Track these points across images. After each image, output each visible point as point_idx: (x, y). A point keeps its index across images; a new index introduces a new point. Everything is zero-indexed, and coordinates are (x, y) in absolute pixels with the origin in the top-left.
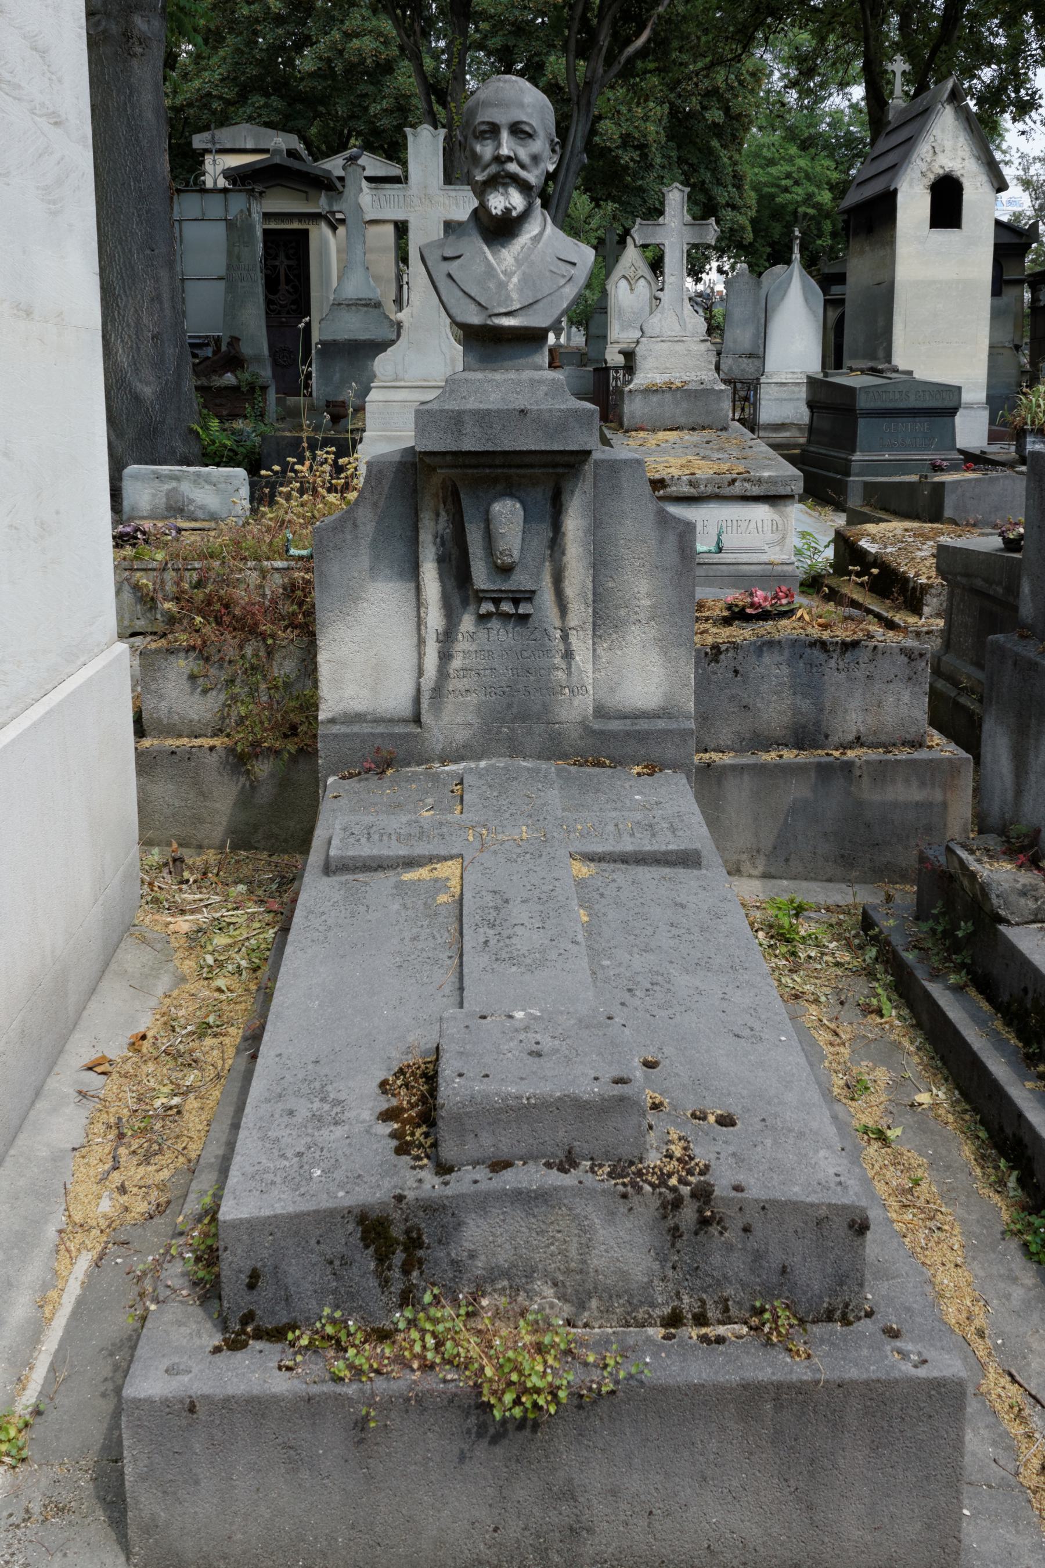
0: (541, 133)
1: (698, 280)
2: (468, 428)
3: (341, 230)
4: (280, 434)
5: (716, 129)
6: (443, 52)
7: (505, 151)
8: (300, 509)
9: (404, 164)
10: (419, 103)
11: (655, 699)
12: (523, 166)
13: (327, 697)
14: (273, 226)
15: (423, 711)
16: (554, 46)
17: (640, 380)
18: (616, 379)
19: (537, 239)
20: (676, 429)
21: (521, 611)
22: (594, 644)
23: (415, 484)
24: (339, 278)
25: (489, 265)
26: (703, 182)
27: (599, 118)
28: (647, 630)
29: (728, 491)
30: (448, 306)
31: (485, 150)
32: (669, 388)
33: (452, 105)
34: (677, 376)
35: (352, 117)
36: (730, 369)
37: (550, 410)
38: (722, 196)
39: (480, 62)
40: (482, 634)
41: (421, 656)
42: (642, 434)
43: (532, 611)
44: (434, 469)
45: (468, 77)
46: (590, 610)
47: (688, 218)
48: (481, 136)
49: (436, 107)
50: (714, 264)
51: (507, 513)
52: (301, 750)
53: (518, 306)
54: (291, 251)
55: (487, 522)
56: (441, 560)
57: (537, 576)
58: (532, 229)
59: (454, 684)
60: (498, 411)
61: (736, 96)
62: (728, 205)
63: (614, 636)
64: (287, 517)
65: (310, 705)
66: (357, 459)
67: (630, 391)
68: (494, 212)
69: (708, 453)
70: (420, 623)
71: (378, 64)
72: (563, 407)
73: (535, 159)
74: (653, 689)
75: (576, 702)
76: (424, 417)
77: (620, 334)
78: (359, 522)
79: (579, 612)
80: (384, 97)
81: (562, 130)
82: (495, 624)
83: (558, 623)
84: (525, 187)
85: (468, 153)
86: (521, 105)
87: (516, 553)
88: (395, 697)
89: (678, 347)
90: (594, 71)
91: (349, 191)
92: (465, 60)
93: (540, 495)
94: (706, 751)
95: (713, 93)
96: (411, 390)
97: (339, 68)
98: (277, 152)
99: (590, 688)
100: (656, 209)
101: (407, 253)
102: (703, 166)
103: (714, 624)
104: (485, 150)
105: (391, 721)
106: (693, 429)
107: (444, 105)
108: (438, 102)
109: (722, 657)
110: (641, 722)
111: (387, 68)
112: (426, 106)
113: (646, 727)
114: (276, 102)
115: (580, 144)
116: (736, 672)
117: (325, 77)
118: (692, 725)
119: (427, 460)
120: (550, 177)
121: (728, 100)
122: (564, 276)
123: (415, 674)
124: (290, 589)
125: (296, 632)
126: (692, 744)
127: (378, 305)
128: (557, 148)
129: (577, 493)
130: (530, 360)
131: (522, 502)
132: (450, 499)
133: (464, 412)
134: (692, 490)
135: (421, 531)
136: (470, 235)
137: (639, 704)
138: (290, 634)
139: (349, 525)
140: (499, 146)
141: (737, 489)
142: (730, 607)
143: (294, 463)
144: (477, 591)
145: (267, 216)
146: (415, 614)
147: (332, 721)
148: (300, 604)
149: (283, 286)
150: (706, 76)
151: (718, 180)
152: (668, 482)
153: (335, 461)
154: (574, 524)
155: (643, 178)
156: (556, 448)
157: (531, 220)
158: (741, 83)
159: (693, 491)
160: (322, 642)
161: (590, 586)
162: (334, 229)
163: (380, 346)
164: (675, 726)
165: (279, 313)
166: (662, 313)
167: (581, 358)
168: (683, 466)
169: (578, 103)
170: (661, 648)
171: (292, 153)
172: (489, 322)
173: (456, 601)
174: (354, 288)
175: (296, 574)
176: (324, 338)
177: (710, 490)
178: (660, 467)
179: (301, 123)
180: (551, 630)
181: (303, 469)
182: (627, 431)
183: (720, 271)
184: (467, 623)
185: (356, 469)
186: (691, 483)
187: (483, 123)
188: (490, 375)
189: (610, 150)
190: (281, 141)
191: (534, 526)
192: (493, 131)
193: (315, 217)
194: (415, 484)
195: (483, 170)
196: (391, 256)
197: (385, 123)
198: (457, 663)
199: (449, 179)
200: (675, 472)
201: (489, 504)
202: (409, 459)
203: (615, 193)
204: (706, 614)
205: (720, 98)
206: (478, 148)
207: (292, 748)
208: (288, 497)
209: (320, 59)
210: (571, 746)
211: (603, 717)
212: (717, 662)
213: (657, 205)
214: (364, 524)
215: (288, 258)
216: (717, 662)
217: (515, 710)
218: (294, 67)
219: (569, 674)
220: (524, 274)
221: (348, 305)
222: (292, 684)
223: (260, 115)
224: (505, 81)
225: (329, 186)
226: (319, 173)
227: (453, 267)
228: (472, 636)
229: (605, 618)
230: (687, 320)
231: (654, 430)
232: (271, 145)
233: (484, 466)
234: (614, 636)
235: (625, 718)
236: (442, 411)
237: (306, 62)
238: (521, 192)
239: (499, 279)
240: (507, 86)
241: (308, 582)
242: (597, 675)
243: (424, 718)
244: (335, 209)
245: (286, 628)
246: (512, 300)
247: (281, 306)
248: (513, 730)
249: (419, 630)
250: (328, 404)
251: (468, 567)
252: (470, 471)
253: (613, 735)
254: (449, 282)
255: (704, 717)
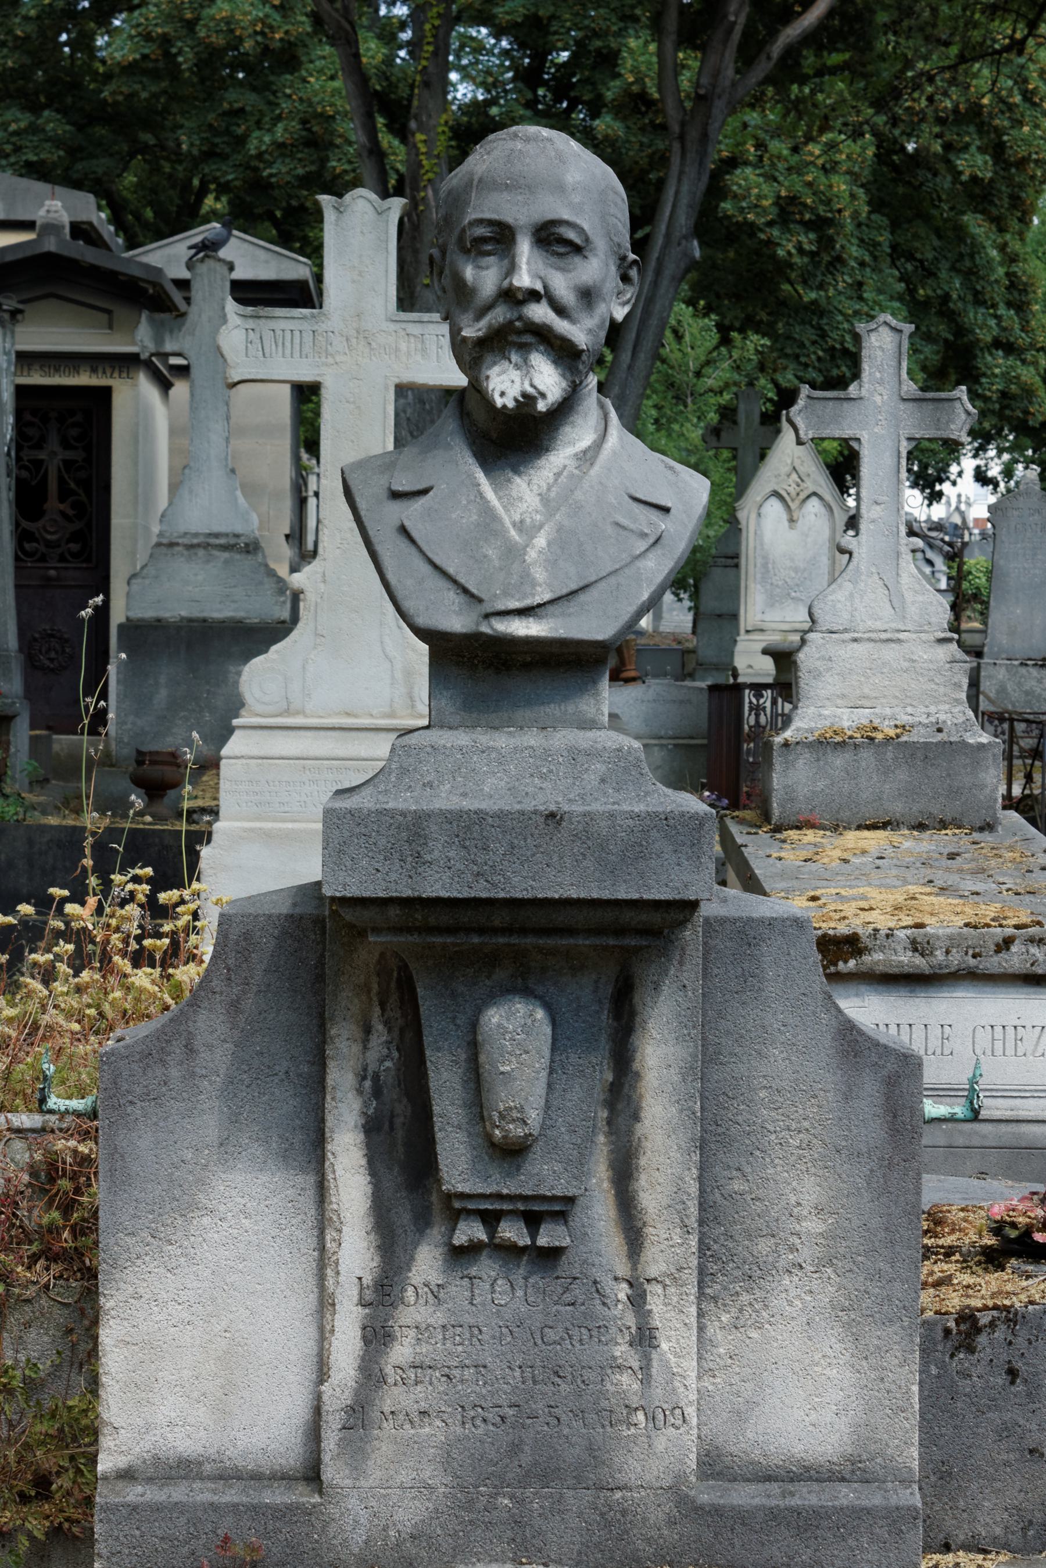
0: (600, 244)
1: (935, 497)
2: (437, 850)
3: (180, 389)
4: (36, 818)
5: (978, 195)
6: (403, 26)
7: (524, 279)
8: (74, 1002)
9: (314, 251)
10: (350, 129)
11: (834, 1438)
12: (561, 311)
13: (117, 1422)
14: (37, 379)
15: (326, 1458)
16: (636, 19)
17: (808, 720)
18: (757, 709)
19: (588, 457)
20: (884, 826)
21: (542, 1241)
22: (701, 1314)
23: (321, 963)
24: (174, 488)
25: (487, 511)
26: (946, 298)
27: (732, 163)
28: (815, 1285)
29: (994, 963)
30: (399, 595)
31: (484, 277)
32: (868, 738)
33: (420, 137)
34: (887, 715)
35: (210, 154)
36: (1002, 690)
37: (612, 815)
38: (983, 326)
39: (479, 48)
40: (458, 1289)
41: (323, 1335)
42: (810, 836)
43: (566, 1242)
44: (362, 933)
45: (454, 76)
46: (694, 1242)
47: (910, 388)
48: (475, 248)
49: (387, 140)
50: (969, 464)
51: (517, 1033)
52: (56, 1532)
53: (547, 597)
54: (74, 432)
55: (474, 1047)
56: (373, 1128)
57: (579, 1166)
58: (578, 436)
59: (394, 1398)
60: (501, 815)
61: (1019, 123)
62: (997, 344)
63: (745, 1298)
64: (45, 1019)
65: (81, 1433)
66: (197, 894)
67: (786, 744)
68: (499, 402)
69: (953, 879)
70: (324, 1262)
71: (266, 51)
72: (639, 808)
73: (588, 295)
74: (828, 1416)
75: (660, 1443)
76: (346, 827)
77: (765, 615)
78: (198, 1043)
79: (668, 1246)
80: (279, 118)
81: (642, 217)
82: (486, 1267)
83: (622, 1269)
84: (565, 353)
85: (446, 281)
86: (560, 188)
87: (534, 1116)
88: (265, 1426)
89: (890, 653)
90: (716, 74)
91: (200, 311)
92: (447, 46)
93: (587, 992)
94: (947, 1548)
95: (972, 115)
96: (313, 756)
97: (186, 59)
98: (51, 228)
99: (691, 1411)
100: (846, 352)
101: (317, 431)
102: (945, 265)
103: (965, 1265)
104: (484, 277)
105: (256, 1477)
106: (921, 827)
107: (403, 134)
108: (390, 128)
109: (982, 1339)
110: (803, 1488)
111: (287, 58)
112: (363, 139)
113: (813, 1500)
114: (52, 122)
115: (684, 221)
116: (1013, 1373)
117: (155, 75)
118: (912, 1497)
119: (348, 915)
120: (615, 332)
121: (999, 132)
122: (644, 535)
123: (310, 1374)
124: (48, 1175)
125: (56, 1268)
126: (916, 1537)
127: (252, 548)
128: (634, 273)
129: (667, 988)
130: (571, 708)
131: (548, 1007)
132: (394, 999)
133: (429, 815)
134: (918, 960)
135: (331, 1065)
136: (448, 447)
137: (798, 1450)
138: (42, 1274)
139: (177, 1049)
140: (512, 269)
141: (1016, 959)
142: (998, 1228)
143: (64, 900)
144: (449, 1197)
145: (25, 359)
146: (313, 1242)
147: (127, 1475)
148: (67, 1208)
149: (53, 504)
150: (953, 81)
151: (976, 293)
152: (866, 941)
153: (152, 898)
154: (660, 1054)
155: (821, 287)
156: (622, 895)
157: (577, 419)
158: (1028, 96)
159: (919, 963)
160: (111, 1300)
161: (694, 1188)
162: (165, 386)
163: (260, 636)
164: (877, 1500)
165: (43, 559)
166: (854, 582)
167: (682, 662)
168: (898, 908)
169: (682, 138)
170: (847, 1325)
171: (81, 231)
172: (485, 629)
173: (404, 1217)
174: (208, 509)
175: (60, 1144)
176: (137, 614)
177: (956, 959)
178: (849, 909)
179: (100, 165)
180: (608, 1284)
181: (80, 913)
182: (778, 829)
183: (981, 477)
184: (426, 1264)
185: (195, 916)
186: (915, 946)
187: (480, 222)
188: (484, 738)
189: (751, 229)
190: (57, 207)
191: (573, 1058)
192: (502, 237)
193: (127, 363)
194: (321, 963)
195: (479, 317)
196: (285, 443)
197: (279, 170)
198: (401, 1352)
199: (408, 299)
200: (882, 921)
201: (479, 1011)
202: (309, 909)
203: (763, 316)
204: (948, 1241)
205: (982, 128)
206: (469, 273)
207: (37, 1527)
208: (48, 976)
209: (148, 37)
210: (648, 1541)
211: (719, 1475)
212: (971, 1350)
213: (850, 346)
214: (210, 1047)
215: (66, 445)
216: (971, 1350)
217: (526, 1459)
218: (91, 49)
219: (646, 1380)
220: (560, 529)
221: (191, 547)
222: (43, 1383)
223: (17, 149)
224: (527, 140)
225: (160, 300)
226: (137, 272)
227: (411, 513)
228: (437, 1293)
229: (725, 1258)
230: (909, 596)
231: (836, 828)
232: (40, 215)
233: (468, 930)
234: (745, 1298)
235: (769, 1479)
236: (379, 812)
237: (115, 43)
238: (557, 362)
239: (507, 539)
240: (531, 148)
241: (85, 1161)
242: (707, 1383)
243: (328, 1473)
244: (169, 347)
245: (34, 1258)
246: (534, 584)
247: (48, 544)
248: (519, 1502)
249: (321, 1278)
250: (141, 757)
251: (430, 1142)
252: (438, 940)
253: (741, 1517)
254: (403, 544)
255: (941, 1474)
